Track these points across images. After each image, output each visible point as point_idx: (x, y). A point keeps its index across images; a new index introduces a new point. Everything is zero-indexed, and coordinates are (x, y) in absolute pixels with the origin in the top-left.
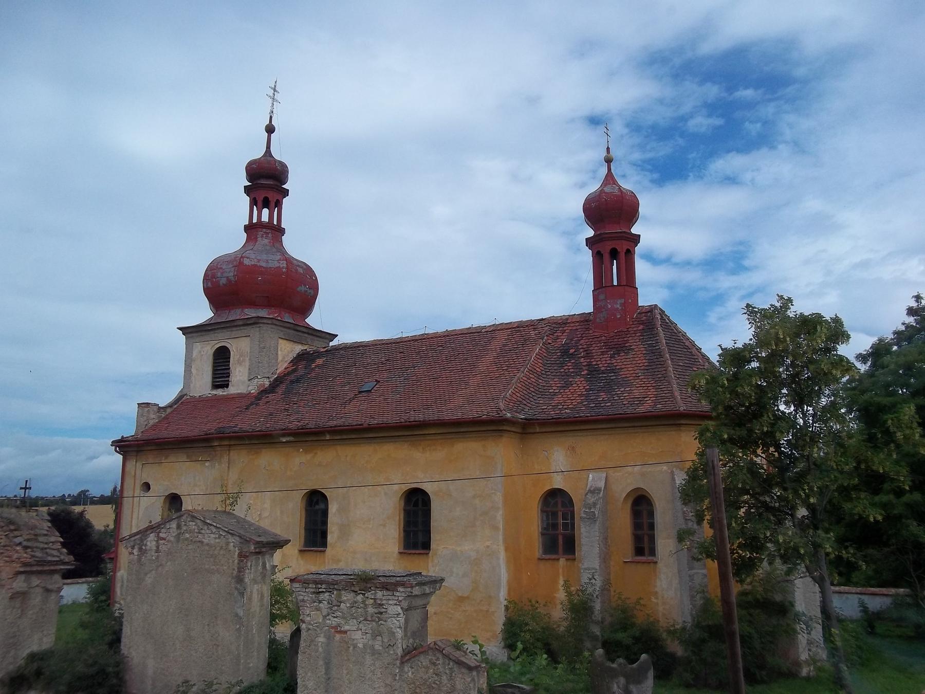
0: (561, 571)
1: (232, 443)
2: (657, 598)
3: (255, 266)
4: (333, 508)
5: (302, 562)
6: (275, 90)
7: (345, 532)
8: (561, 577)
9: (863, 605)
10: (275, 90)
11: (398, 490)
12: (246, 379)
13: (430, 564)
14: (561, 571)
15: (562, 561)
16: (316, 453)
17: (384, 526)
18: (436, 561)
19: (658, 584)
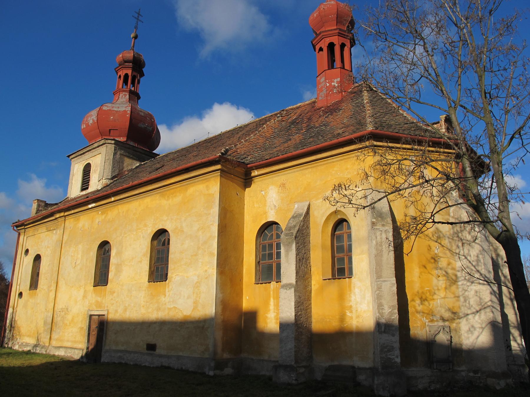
0: (272, 293)
1: (66, 214)
2: (351, 312)
3: (110, 110)
4: (113, 253)
5: (94, 295)
6: (139, 14)
7: (119, 271)
8: (272, 299)
9: (338, 5)
10: (139, 14)
11: (151, 231)
12: (97, 181)
13: (167, 290)
14: (272, 293)
15: (273, 283)
16: (107, 214)
17: (141, 262)
18: (170, 287)
19: (353, 298)
